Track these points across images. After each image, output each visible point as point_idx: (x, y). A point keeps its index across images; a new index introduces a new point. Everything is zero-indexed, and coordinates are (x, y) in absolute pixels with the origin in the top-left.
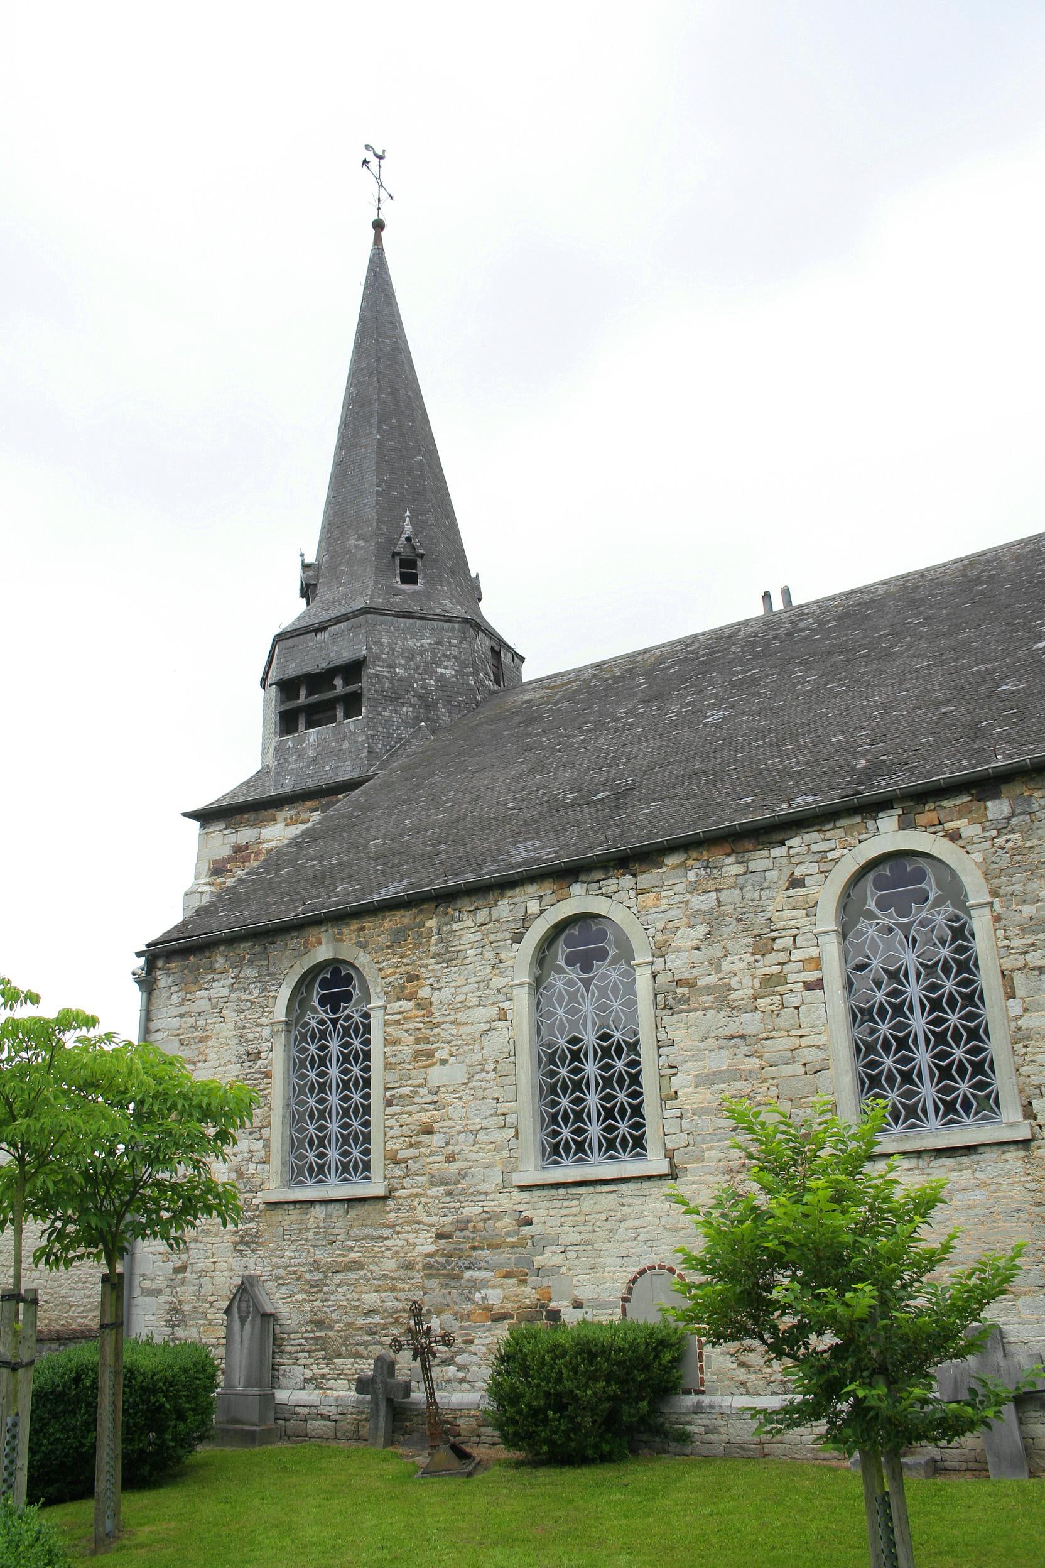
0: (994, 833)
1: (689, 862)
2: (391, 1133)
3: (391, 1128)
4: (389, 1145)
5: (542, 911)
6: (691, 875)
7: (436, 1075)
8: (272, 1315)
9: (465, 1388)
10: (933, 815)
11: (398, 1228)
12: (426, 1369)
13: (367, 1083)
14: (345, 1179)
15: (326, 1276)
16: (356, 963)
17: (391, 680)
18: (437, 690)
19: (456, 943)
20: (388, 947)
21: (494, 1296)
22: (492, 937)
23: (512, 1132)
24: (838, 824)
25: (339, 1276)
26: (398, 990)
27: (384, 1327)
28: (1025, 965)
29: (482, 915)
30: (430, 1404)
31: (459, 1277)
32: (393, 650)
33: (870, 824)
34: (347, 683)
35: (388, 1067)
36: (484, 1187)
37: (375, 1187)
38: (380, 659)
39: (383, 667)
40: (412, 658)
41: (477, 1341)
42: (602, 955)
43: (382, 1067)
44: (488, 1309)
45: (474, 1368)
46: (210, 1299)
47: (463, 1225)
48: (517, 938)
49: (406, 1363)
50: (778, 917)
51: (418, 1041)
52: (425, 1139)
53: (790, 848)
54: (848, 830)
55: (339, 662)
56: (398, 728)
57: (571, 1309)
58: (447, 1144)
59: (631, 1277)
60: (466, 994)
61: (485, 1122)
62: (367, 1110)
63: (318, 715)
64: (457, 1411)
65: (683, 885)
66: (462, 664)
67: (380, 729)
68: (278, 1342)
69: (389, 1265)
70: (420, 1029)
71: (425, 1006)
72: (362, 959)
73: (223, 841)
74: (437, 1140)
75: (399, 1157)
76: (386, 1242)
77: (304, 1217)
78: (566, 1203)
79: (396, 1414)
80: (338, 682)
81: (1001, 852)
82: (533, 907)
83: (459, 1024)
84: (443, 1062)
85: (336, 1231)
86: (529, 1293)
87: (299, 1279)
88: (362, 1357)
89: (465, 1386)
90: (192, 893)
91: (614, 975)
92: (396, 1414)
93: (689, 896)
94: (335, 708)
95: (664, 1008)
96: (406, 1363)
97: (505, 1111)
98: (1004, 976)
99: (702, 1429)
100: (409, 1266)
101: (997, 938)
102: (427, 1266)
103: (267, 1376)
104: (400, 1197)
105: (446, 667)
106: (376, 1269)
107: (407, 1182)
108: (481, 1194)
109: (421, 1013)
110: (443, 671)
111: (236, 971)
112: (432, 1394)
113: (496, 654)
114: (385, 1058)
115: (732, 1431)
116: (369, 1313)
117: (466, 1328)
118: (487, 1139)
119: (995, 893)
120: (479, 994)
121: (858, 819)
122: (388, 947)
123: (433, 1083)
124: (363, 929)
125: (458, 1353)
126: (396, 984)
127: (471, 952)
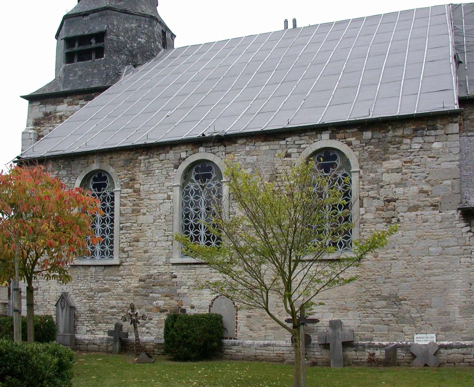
0: (364, 145)
1: (247, 143)
2: (122, 241)
3: (122, 238)
4: (121, 245)
5: (187, 157)
6: (247, 148)
7: (141, 219)
8: (74, 307)
9: (152, 332)
10: (343, 135)
11: (124, 277)
12: (135, 327)
13: (112, 221)
14: (103, 257)
15: (95, 294)
16: (109, 172)
17: (117, 42)
18: (137, 49)
19: (151, 167)
20: (123, 166)
21: (161, 303)
22: (166, 166)
23: (171, 243)
24: (306, 134)
25: (100, 294)
26: (126, 184)
27: (118, 313)
28: (368, 196)
29: (162, 156)
30: (136, 340)
31: (147, 296)
32: (118, 28)
33: (319, 136)
34: (97, 42)
35: (121, 215)
36: (159, 263)
37: (116, 261)
38: (112, 32)
39: (114, 36)
40: (127, 32)
41: (154, 319)
42: (209, 176)
43: (119, 214)
44: (158, 308)
45: (153, 328)
46: (48, 300)
47: (150, 276)
48: (176, 167)
49: (127, 326)
50: (280, 168)
51: (134, 205)
52: (136, 243)
53: (287, 141)
54: (310, 137)
55: (94, 32)
56: (120, 65)
57: (190, 309)
58: (145, 246)
59: (213, 298)
60: (154, 188)
61: (160, 238)
62: (112, 231)
63: (84, 56)
64: (146, 343)
65: (244, 152)
66: (149, 37)
67: (112, 65)
68: (76, 317)
69: (120, 290)
70: (135, 201)
71: (137, 191)
72: (111, 171)
73: (40, 110)
74: (141, 244)
75: (125, 250)
76: (119, 282)
77: (86, 271)
78: (190, 271)
79: (123, 344)
80: (93, 41)
81: (365, 152)
82: (183, 155)
83: (151, 200)
84: (144, 214)
85: (99, 277)
86: (174, 303)
87: (84, 294)
88: (109, 323)
89: (149, 334)
90: (25, 133)
91: (214, 185)
92: (123, 344)
93: (246, 157)
94: (91, 53)
95: (233, 200)
96: (127, 326)
97: (168, 234)
98: (360, 199)
99: (235, 351)
100: (128, 291)
101: (359, 185)
102: (134, 292)
103: (73, 328)
104: (125, 265)
105: (142, 38)
106: (115, 292)
107: (128, 260)
108: (157, 266)
109: (136, 194)
110: (140, 40)
111: (58, 171)
112: (138, 336)
113: (164, 33)
114: (120, 211)
115: (246, 352)
116: (112, 308)
117: (150, 314)
118: (160, 245)
119: (361, 168)
120: (160, 188)
121: (314, 133)
122: (123, 166)
123: (139, 222)
124: (112, 158)
125: (146, 323)
126: (125, 182)
127: (158, 171)
